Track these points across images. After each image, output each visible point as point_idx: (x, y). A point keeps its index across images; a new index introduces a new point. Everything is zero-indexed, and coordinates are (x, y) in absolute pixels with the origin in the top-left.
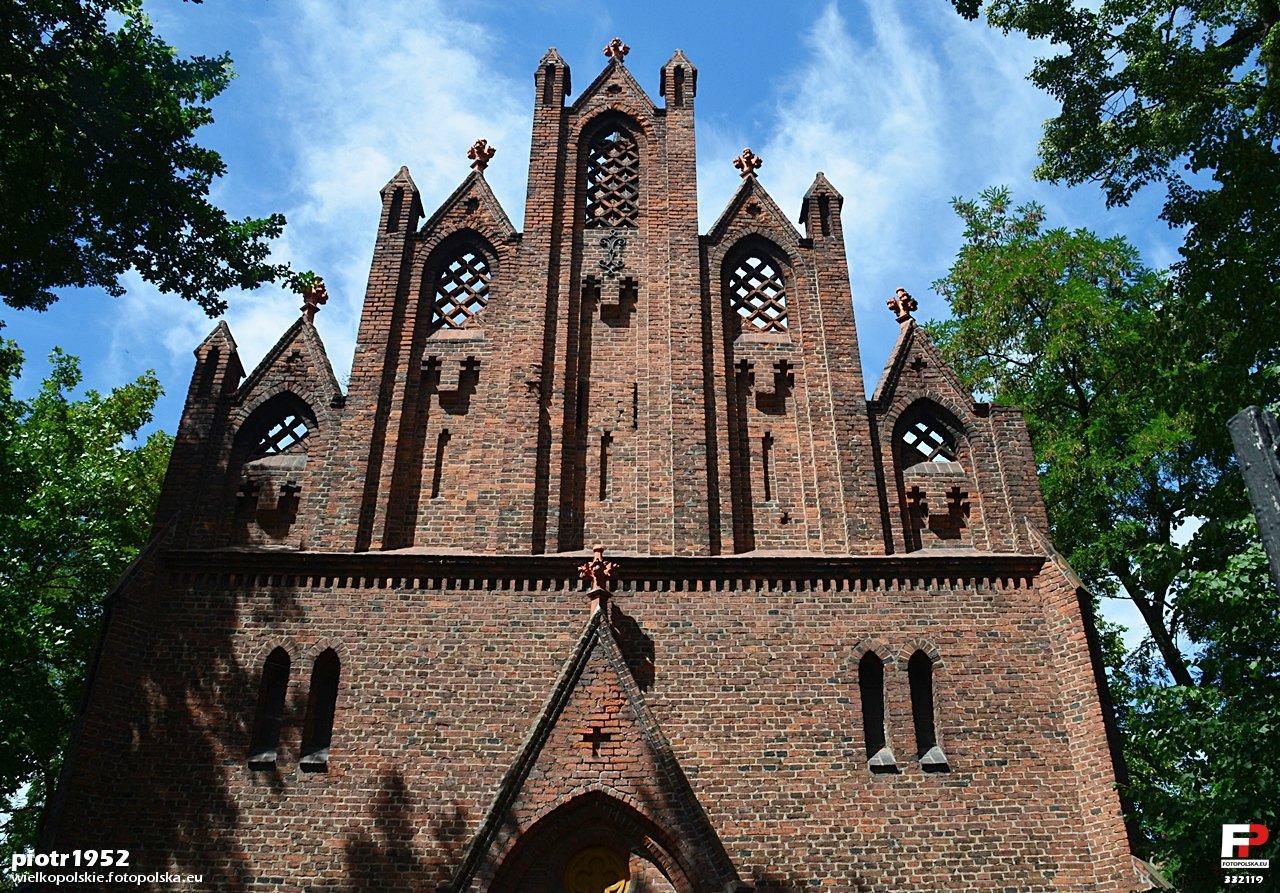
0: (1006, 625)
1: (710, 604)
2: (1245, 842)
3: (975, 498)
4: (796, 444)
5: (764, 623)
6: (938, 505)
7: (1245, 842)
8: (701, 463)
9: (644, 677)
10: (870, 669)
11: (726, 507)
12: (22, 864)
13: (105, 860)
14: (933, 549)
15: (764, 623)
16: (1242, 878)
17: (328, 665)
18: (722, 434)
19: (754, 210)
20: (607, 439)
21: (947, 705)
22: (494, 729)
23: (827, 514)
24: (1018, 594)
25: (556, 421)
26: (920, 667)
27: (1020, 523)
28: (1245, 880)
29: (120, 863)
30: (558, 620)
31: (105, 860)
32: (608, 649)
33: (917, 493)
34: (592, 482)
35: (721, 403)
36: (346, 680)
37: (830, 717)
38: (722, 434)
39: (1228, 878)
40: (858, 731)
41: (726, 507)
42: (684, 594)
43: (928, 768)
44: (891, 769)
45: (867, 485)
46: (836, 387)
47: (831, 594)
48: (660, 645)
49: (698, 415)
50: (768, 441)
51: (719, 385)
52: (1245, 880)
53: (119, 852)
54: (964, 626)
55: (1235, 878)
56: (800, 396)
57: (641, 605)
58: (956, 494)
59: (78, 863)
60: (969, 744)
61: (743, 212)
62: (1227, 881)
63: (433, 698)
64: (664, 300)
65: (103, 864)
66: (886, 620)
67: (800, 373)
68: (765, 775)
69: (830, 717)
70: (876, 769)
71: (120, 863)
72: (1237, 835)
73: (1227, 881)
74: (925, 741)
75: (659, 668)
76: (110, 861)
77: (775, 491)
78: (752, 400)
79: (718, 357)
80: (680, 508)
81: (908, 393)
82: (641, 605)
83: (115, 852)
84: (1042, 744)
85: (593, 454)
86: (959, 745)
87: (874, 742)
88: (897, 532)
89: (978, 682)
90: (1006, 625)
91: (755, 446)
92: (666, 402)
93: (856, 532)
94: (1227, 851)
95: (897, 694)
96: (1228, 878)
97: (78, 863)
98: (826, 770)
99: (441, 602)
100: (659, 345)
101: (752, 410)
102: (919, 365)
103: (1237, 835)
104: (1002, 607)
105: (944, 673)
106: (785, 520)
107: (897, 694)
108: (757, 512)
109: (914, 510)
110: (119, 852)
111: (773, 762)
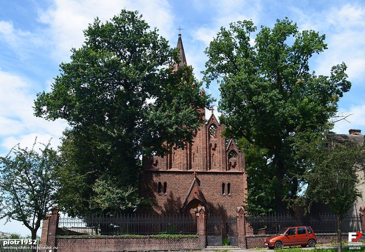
0: (239, 180)
1: (206, 177)
2: (355, 237)
3: (237, 163)
4: (217, 155)
5: (212, 179)
6: (233, 164)
7: (355, 237)
8: (206, 159)
9: (199, 185)
10: (223, 185)
11: (208, 165)
12: (6, 244)
13: (30, 243)
14: (232, 170)
15: (212, 179)
16: (354, 248)
17: (165, 184)
18: (208, 155)
19: (213, 119)
20: (194, 154)
21: (231, 189)
22: (184, 191)
23: (220, 165)
24: (241, 176)
25: (188, 152)
26: (229, 185)
27: (242, 167)
28: (355, 248)
29: (34, 244)
30: (191, 180)
31: (30, 243)
32: (197, 184)
33: (231, 162)
34: (192, 160)
35: (208, 150)
36: (167, 185)
37: (219, 190)
38: (208, 155)
39: (350, 248)
40: (222, 192)
41: (208, 165)
42: (204, 176)
43: (229, 196)
44: (225, 196)
45: (225, 162)
46: (222, 149)
47: (220, 176)
48: (201, 182)
49: (205, 152)
50: (213, 154)
51: (208, 148)
52: (355, 248)
53: (34, 240)
54: (234, 180)
55: (352, 248)
56: (217, 149)
57: (199, 177)
58: (235, 163)
59: (22, 243)
60: (233, 193)
61: (211, 120)
62: (350, 249)
63: (177, 187)
64: (201, 134)
65: (29, 244)
66: (226, 179)
67: (218, 145)
68: (212, 196)
69: (219, 190)
70: (223, 196)
71: (34, 244)
72: (353, 235)
73: (350, 249)
74: (229, 193)
75: (201, 184)
76: (31, 243)
77: (214, 161)
78: (211, 149)
79: (208, 143)
80: (203, 165)
81: (231, 149)
82: (199, 177)
83: (33, 240)
84: (241, 194)
85: (192, 156)
86: (232, 193)
87: (223, 192)
88: (228, 168)
89: (235, 187)
90: (239, 180)
91: (212, 155)
92: (201, 150)
93: (223, 168)
94: (350, 240)
95: (226, 188)
96: (350, 248)
97: (22, 243)
98: (218, 196)
99: (177, 176)
100: (200, 141)
101: (211, 150)
102: (233, 145)
103: (353, 235)
104: (239, 178)
105: (231, 185)
106: (215, 165)
107: (226, 188)
108: (212, 164)
109: (230, 164)
110: (34, 240)
111: (213, 195)
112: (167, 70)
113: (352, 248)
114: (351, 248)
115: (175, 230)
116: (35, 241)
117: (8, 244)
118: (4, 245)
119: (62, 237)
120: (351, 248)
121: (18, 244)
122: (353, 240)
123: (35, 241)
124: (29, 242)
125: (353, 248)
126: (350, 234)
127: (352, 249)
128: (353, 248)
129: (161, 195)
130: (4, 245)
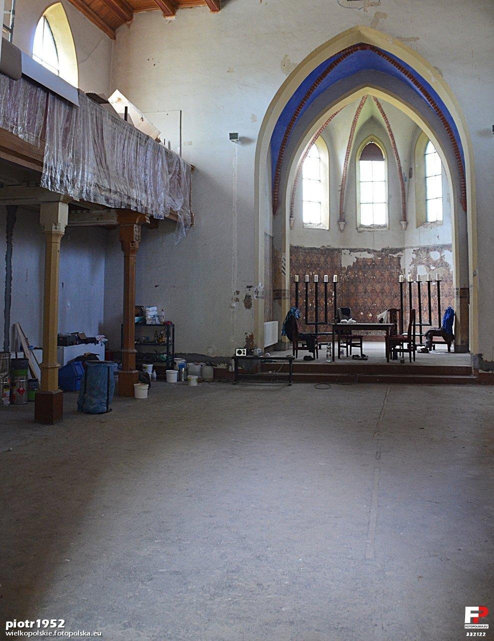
7: (476, 615)
12: (11, 626)
13: (52, 625)
28: (477, 634)
29: (60, 626)
31: (52, 625)
39: (468, 633)
52: (477, 634)
53: (59, 620)
59: (39, 626)
65: (51, 626)
72: (472, 612)
94: (467, 620)
97: (39, 626)
103: (472, 612)
110: (59, 620)
112: (346, 377)
113: (471, 633)
114: (470, 634)
115: (136, 185)
116: (61, 622)
117: (15, 626)
118: (7, 629)
119: (468, 366)
120: (470, 634)
121: (31, 626)
122: (473, 620)
123: (61, 622)
124: (52, 623)
125: (473, 634)
126: (468, 609)
127: (471, 635)
128: (473, 634)
129: (364, 586)
130: (7, 629)
